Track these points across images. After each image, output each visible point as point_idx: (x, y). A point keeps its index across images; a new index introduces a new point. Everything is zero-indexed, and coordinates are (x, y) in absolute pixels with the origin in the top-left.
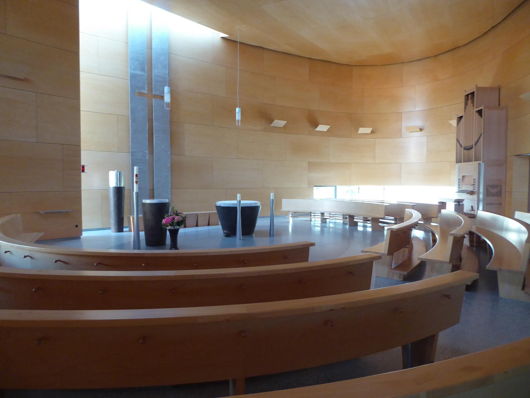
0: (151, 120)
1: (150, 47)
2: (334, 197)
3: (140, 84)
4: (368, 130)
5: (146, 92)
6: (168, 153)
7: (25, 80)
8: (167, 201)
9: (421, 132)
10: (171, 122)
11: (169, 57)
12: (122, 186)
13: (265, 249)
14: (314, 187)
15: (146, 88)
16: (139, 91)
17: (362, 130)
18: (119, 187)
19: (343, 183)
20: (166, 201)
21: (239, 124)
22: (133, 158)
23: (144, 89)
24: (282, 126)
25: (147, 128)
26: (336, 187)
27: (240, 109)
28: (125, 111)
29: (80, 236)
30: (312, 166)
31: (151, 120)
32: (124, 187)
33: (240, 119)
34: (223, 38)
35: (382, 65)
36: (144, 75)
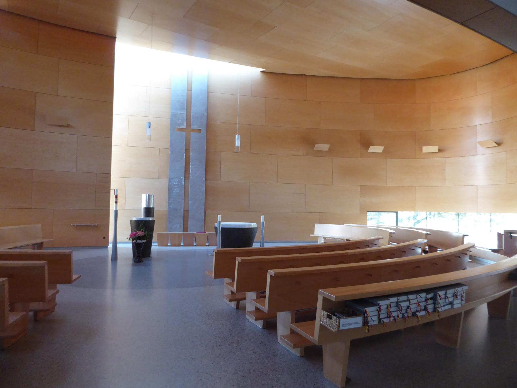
0: (187, 151)
1: (189, 89)
2: (395, 225)
3: (180, 121)
4: (434, 149)
5: (184, 127)
6: (203, 179)
7: (68, 126)
8: (253, 225)
9: (499, 147)
10: (207, 152)
11: (208, 95)
12: (152, 206)
13: (424, 285)
14: (368, 213)
15: (185, 124)
16: (178, 127)
17: (426, 149)
18: (148, 208)
19: (405, 208)
20: (251, 225)
21: (238, 150)
22: (170, 183)
23: (183, 125)
24: (327, 150)
25: (184, 158)
26: (397, 213)
27: (239, 136)
28: (166, 145)
29: (108, 246)
30: (364, 190)
31: (187, 151)
32: (153, 208)
33: (239, 145)
34: (262, 72)
35: (451, 74)
36: (184, 113)
